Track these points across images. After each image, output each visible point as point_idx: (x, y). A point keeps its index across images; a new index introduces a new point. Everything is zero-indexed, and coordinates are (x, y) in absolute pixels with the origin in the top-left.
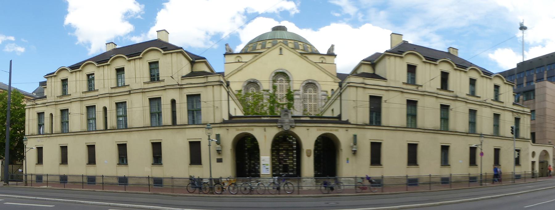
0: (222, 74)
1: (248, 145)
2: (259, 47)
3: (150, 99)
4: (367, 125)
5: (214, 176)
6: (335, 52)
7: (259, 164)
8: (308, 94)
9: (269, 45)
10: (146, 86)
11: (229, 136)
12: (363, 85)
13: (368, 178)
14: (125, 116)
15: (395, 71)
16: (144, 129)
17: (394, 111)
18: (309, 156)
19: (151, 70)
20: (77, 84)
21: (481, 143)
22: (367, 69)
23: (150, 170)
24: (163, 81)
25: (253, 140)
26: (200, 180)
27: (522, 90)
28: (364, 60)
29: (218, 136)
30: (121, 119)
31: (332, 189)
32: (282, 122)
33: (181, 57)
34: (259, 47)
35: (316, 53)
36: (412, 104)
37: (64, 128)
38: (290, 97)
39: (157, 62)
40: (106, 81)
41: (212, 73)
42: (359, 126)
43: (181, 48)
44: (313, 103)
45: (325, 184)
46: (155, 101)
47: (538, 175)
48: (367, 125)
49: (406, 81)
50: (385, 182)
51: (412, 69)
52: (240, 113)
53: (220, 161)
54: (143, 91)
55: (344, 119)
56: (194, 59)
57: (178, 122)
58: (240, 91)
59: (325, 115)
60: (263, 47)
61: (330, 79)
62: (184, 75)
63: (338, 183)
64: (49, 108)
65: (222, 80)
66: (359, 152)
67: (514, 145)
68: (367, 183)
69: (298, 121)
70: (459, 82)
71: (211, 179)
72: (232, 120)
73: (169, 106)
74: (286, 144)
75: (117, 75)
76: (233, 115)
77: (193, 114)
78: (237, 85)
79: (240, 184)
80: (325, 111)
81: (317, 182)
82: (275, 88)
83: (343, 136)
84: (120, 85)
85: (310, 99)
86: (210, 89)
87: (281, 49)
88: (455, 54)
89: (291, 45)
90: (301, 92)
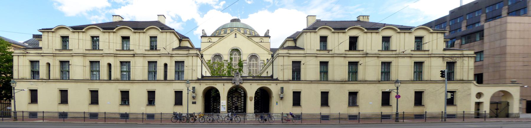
0: (199, 49)
1: (213, 94)
2: (222, 32)
3: (149, 62)
4: (290, 80)
5: (190, 112)
6: (270, 35)
7: (220, 105)
8: (252, 62)
9: (228, 32)
10: (147, 53)
11: (201, 88)
12: (288, 55)
13: (291, 114)
14: (129, 72)
15: (311, 42)
16: (143, 81)
17: (310, 70)
18: (251, 100)
19: (151, 42)
20: (80, 43)
21: (397, 88)
22: (291, 44)
23: (145, 109)
24: (159, 50)
25: (217, 91)
26: (180, 115)
27: (459, 33)
28: (288, 38)
29: (194, 88)
30: (125, 73)
31: (266, 120)
32: (235, 80)
33: (173, 36)
34: (222, 32)
35: (258, 36)
36: (324, 64)
37: (64, 76)
38: (241, 65)
39: (156, 37)
40: (111, 45)
41: (193, 48)
42: (284, 81)
43: (173, 29)
44: (255, 68)
45: (261, 117)
46: (152, 64)
47: (489, 116)
48: (290, 80)
49: (319, 49)
50: (303, 117)
51: (324, 39)
52: (208, 74)
53: (194, 103)
54: (144, 56)
55: (275, 77)
56: (181, 38)
57: (168, 78)
58: (210, 61)
59: (262, 75)
60: (225, 33)
61: (266, 52)
62: (174, 48)
63: (270, 116)
64: (45, 58)
65: (198, 53)
66: (285, 98)
67: (446, 88)
68: (290, 117)
69: (245, 79)
70: (370, 42)
71: (187, 114)
72: (203, 78)
73: (162, 68)
74: (237, 93)
75: (123, 41)
76: (204, 75)
77: (179, 73)
78: (208, 57)
79: (206, 117)
80: (262, 73)
81: (256, 116)
82: (231, 59)
83: (274, 88)
84: (125, 49)
85: (253, 65)
86: (190, 58)
87: (236, 34)
88: (365, 20)
89: (242, 32)
90: (248, 61)
